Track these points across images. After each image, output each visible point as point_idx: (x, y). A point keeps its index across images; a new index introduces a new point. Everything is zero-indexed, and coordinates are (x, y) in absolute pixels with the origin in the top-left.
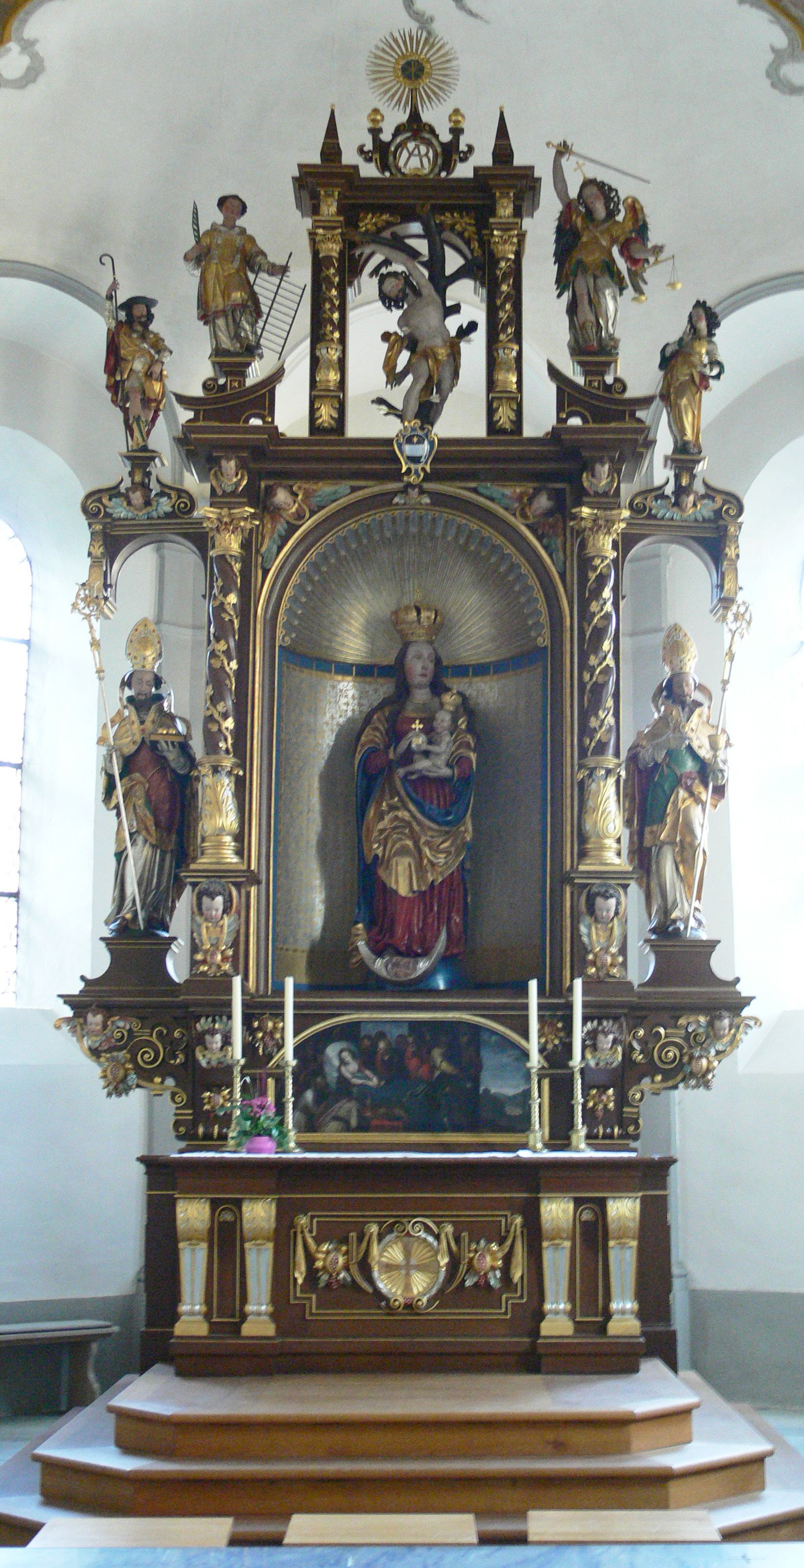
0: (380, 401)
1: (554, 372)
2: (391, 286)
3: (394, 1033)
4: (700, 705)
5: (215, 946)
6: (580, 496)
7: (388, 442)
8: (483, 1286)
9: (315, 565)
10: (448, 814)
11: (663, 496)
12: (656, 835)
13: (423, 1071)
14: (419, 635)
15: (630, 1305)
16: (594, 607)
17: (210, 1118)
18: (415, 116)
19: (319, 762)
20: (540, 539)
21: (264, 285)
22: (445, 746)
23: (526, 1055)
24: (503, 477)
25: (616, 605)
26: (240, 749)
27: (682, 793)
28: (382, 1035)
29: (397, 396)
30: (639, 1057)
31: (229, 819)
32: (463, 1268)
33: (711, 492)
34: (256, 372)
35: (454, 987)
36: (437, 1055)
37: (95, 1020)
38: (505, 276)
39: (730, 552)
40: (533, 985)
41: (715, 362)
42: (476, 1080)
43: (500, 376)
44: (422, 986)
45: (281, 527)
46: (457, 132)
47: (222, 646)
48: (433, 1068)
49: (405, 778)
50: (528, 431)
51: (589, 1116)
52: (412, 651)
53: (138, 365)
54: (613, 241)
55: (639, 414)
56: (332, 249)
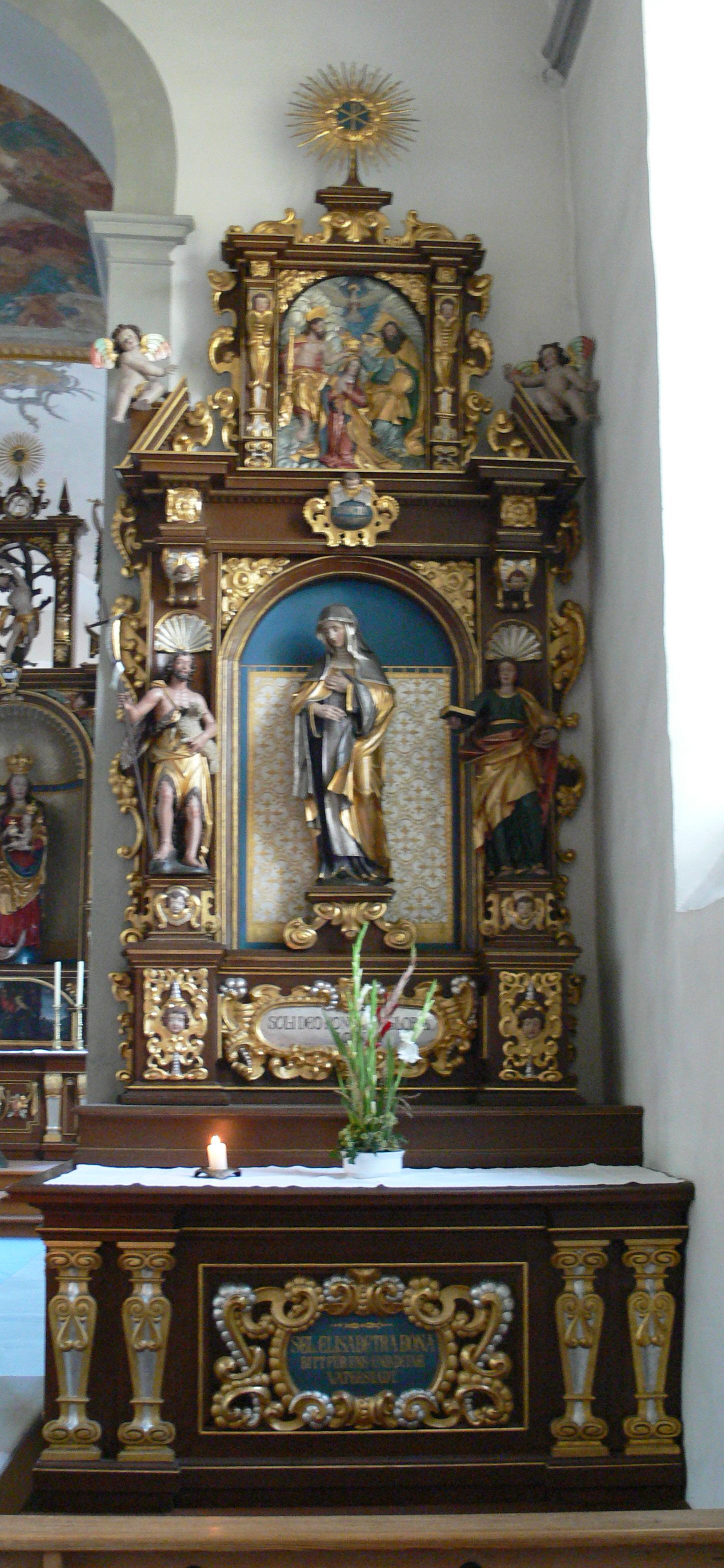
8: (17, 1118)
10: (28, 870)
13: (10, 1008)
14: (19, 771)
18: (19, 483)
20: (80, 719)
22: (27, 834)
24: (60, 686)
32: (7, 1108)
35: (32, 963)
42: (38, 1014)
44: (12, 963)
46: (41, 492)
48: (16, 1006)
49: (6, 851)
52: (15, 780)
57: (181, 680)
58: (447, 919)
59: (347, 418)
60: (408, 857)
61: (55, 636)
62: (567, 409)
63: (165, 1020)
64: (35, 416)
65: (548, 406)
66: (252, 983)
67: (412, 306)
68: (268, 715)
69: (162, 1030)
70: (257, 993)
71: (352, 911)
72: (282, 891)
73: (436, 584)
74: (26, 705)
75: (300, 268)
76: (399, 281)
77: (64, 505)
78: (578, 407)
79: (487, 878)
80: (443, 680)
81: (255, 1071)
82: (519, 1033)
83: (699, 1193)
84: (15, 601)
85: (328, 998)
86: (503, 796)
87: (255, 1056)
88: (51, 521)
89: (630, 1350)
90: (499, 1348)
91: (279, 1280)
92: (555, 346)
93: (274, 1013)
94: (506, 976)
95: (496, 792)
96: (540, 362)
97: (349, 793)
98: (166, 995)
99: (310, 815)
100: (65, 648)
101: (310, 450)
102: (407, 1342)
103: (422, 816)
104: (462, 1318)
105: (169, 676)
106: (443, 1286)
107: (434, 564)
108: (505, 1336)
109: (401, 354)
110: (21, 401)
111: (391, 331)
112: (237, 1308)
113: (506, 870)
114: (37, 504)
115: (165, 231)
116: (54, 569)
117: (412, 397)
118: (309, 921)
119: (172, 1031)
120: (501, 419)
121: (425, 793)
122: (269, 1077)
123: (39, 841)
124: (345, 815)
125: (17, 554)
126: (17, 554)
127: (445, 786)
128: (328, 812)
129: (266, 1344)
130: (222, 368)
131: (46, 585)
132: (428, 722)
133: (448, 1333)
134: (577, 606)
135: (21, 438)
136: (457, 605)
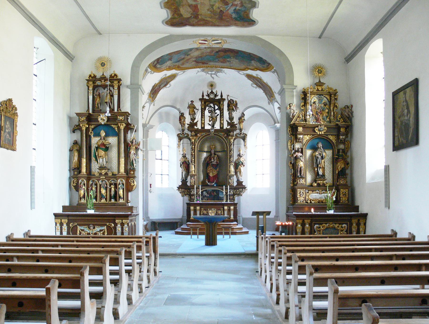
0: (208, 124)
1: (227, 121)
2: (209, 111)
3: (210, 191)
4: (242, 156)
5: (193, 182)
6: (230, 135)
7: (210, 129)
9: (202, 142)
11: (239, 134)
12: (237, 170)
15: (233, 216)
16: (231, 147)
17: (192, 199)
18: (212, 91)
19: (202, 162)
21: (196, 111)
22: (215, 161)
23: (223, 192)
25: (233, 147)
26: (194, 162)
27: (240, 166)
28: (209, 191)
29: (210, 123)
30: (235, 193)
31: (194, 169)
33: (244, 134)
34: (195, 122)
35: (217, 186)
36: (215, 193)
37: (180, 189)
38: (222, 110)
39: (245, 140)
40: (224, 186)
41: (244, 120)
43: (221, 121)
45: (198, 138)
46: (217, 93)
47: (193, 151)
49: (211, 164)
50: (224, 128)
51: (230, 199)
53: (183, 120)
54: (234, 106)
55: (236, 125)
56: (203, 107)
57: (299, 152)
58: (332, 182)
59: (319, 116)
60: (327, 174)
61: (220, 122)
62: (349, 115)
63: (300, 195)
64: (213, 77)
65: (347, 115)
66: (309, 191)
67: (328, 100)
68: (309, 156)
69: (300, 197)
70: (309, 192)
71: (322, 182)
72: (311, 179)
73: (331, 138)
74: (214, 136)
75: (313, 94)
76: (326, 96)
77: (222, 96)
78: (350, 115)
79: (338, 177)
80: (331, 151)
81: (309, 202)
82: (343, 197)
83: (368, 214)
84: (212, 115)
85: (318, 193)
86: (340, 167)
87: (309, 200)
88: (219, 99)
89: (360, 231)
90: (345, 232)
91: (321, 224)
92: (347, 106)
93: (311, 195)
94: (341, 190)
95: (339, 167)
96: (345, 107)
97: (321, 167)
98: (300, 192)
99: (316, 169)
100: (222, 124)
101: (314, 120)
102: (335, 231)
103: (329, 169)
104: (341, 228)
105: (298, 151)
106: (339, 225)
107: (331, 136)
108: (346, 230)
109: (326, 106)
110: (211, 74)
111: (325, 103)
112: (317, 227)
113: (340, 176)
114: (216, 95)
115: (293, 88)
116: (219, 109)
117: (328, 113)
118: (316, 183)
119: (301, 197)
120: (340, 116)
121: (329, 166)
122: (311, 203)
123: (218, 162)
124: (321, 169)
125: (212, 105)
126: (212, 105)
127: (332, 165)
128: (318, 169)
129: (320, 231)
130: (302, 108)
131: (218, 112)
132: (329, 157)
133: (340, 230)
134: (349, 141)
135: (211, 82)
136: (334, 141)
